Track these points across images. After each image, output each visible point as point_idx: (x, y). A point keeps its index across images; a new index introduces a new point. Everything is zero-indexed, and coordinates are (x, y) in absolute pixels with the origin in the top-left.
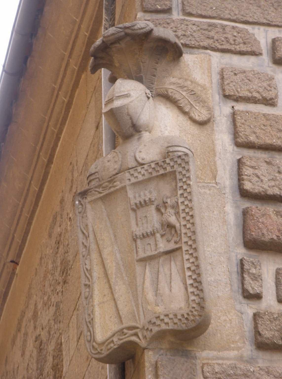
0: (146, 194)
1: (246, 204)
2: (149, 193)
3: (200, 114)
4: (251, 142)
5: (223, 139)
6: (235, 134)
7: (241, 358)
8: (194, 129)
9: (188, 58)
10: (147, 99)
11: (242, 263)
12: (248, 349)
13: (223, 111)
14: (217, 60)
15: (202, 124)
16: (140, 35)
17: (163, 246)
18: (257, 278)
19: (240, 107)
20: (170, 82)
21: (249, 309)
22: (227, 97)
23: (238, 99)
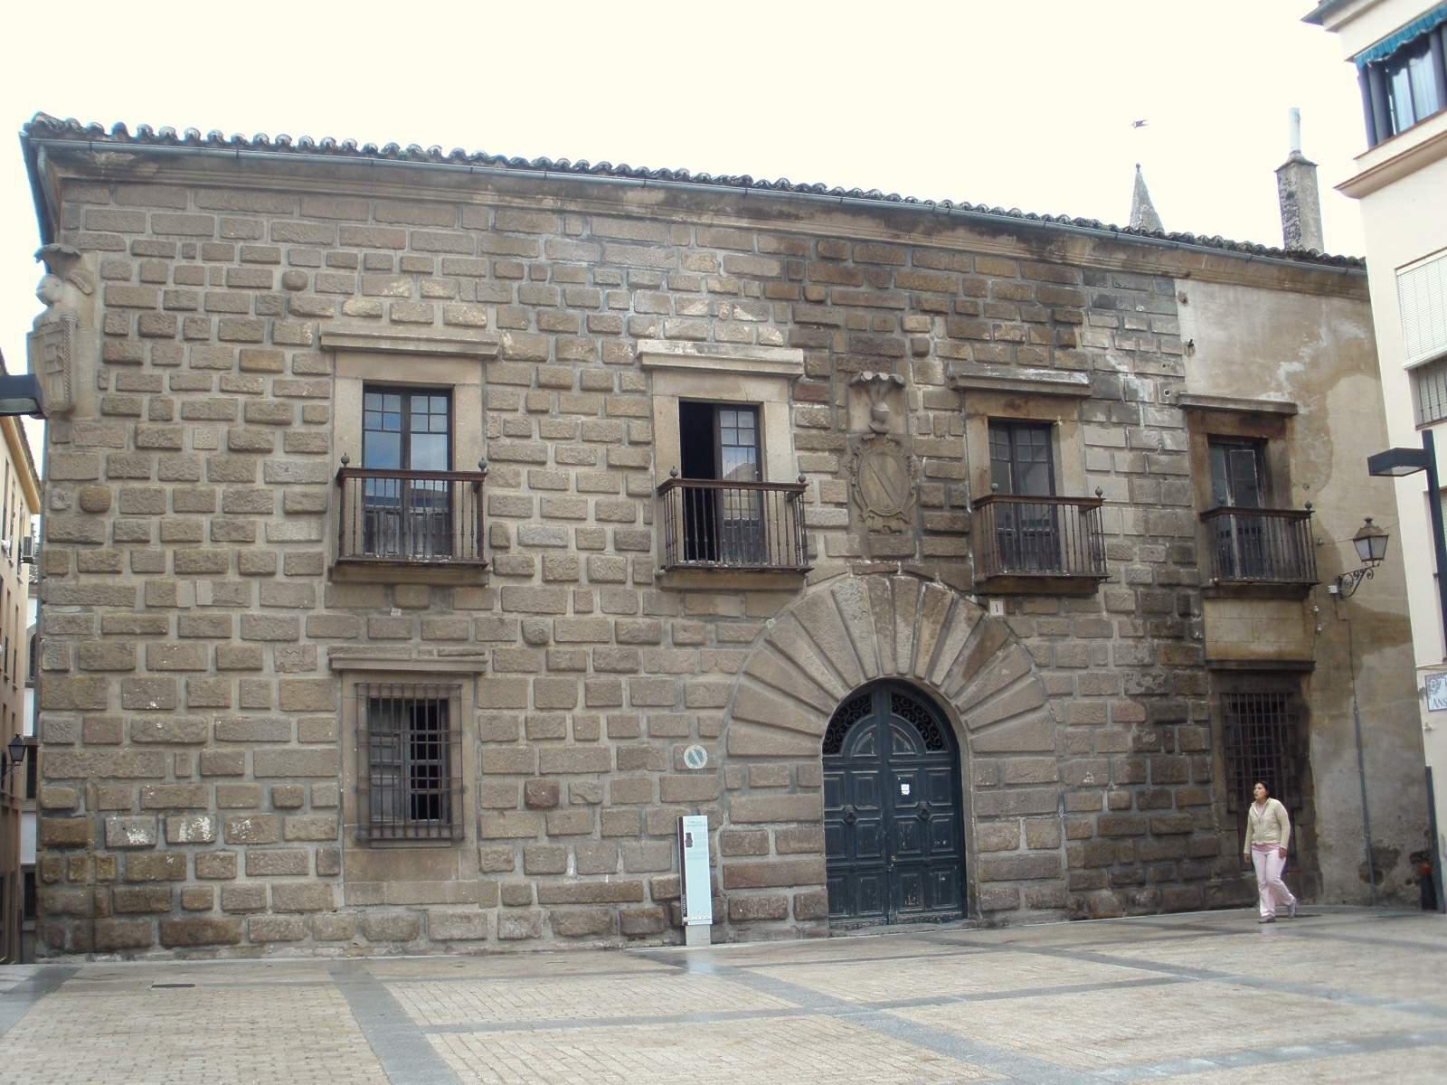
0: (53, 340)
1: (107, 339)
2: (53, 340)
3: (88, 289)
4: (711, 622)
5: (99, 303)
6: (105, 300)
7: (94, 421)
8: (85, 298)
9: (86, 256)
10: (658, 530)
11: (99, 371)
12: (97, 415)
13: (101, 286)
14: (101, 256)
15: (88, 295)
16: (569, 889)
17: (58, 368)
18: (107, 380)
19: (110, 283)
20: (73, 272)
21: (101, 395)
22: (104, 278)
23: (109, 279)
